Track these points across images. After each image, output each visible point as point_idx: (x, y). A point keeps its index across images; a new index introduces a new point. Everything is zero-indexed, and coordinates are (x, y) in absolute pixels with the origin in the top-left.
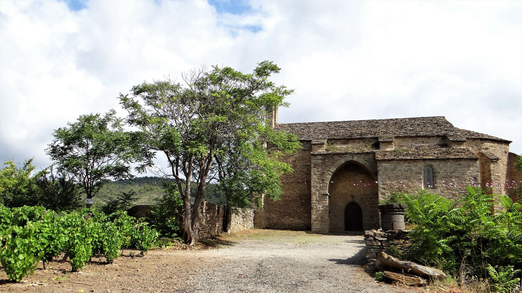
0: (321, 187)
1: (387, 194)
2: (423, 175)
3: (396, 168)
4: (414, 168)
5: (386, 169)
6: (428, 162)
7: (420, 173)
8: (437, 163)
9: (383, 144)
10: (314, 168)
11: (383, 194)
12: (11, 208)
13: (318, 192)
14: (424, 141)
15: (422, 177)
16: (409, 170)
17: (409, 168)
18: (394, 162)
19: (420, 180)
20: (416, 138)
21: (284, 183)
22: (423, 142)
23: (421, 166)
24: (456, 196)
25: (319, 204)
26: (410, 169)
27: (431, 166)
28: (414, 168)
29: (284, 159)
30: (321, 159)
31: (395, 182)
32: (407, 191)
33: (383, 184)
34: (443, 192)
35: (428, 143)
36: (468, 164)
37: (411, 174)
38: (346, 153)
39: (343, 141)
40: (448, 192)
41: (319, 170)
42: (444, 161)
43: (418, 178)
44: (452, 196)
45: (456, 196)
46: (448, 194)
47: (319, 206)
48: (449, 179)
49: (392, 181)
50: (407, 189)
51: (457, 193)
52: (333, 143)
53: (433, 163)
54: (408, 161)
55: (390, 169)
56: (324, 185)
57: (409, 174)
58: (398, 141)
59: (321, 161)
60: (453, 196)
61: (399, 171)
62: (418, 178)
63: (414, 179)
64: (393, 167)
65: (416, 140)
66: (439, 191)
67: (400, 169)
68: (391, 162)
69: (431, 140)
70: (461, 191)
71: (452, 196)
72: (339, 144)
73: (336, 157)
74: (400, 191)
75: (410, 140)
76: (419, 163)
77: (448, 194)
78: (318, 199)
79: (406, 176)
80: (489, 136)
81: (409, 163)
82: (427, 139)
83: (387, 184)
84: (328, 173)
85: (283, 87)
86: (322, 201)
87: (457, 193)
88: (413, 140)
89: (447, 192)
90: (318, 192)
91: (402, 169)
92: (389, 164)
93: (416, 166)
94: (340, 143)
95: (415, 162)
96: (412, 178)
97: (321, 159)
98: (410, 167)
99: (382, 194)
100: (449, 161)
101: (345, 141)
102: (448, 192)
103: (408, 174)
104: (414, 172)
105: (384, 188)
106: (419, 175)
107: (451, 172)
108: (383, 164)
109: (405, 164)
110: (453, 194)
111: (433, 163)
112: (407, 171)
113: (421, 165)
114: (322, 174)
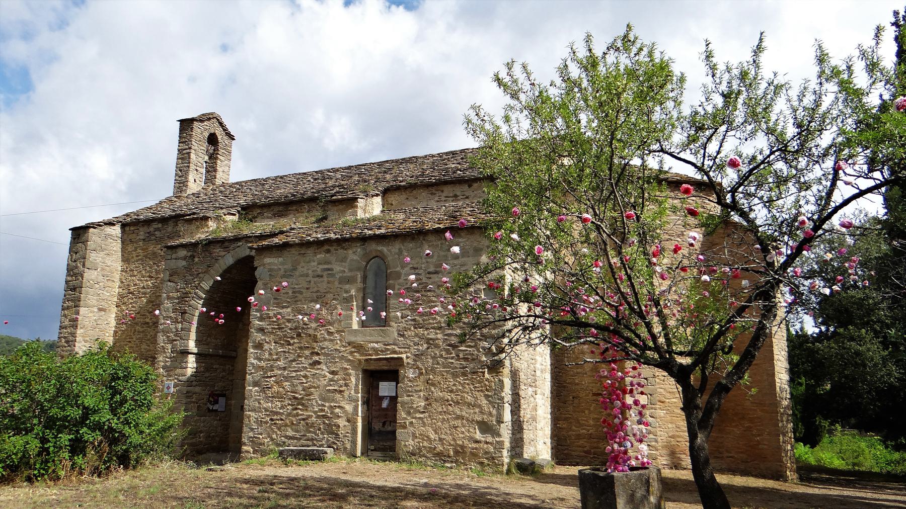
0: (177, 331)
1: (266, 346)
2: (360, 285)
3: (295, 269)
4: (337, 268)
5: (272, 274)
6: (373, 247)
7: (350, 281)
8: (396, 246)
9: (335, 208)
10: (170, 281)
11: (259, 346)
12: (896, 440)
13: (169, 346)
14: (458, 194)
15: (353, 292)
16: (325, 273)
17: (326, 266)
18: (293, 251)
19: (348, 300)
20: (440, 188)
21: (148, 323)
22: (456, 196)
23: (355, 258)
24: (437, 346)
25: (171, 376)
26: (329, 269)
27: (381, 257)
28: (337, 268)
29: (154, 264)
30: (185, 258)
31: (289, 310)
32: (315, 336)
33: (261, 319)
34: (403, 336)
35: (467, 198)
36: (475, 244)
37: (329, 285)
38: (237, 239)
39: (276, 209)
40: (417, 335)
41: (179, 287)
42: (413, 239)
43: (345, 295)
44: (425, 346)
45: (437, 346)
46: (416, 339)
47: (169, 382)
48: (424, 293)
49: (283, 307)
50: (316, 329)
51: (439, 336)
52: (256, 217)
53: (385, 249)
54: (326, 247)
55: (282, 272)
56: (186, 325)
57: (325, 285)
58: (398, 198)
59: (184, 263)
60: (428, 348)
61: (301, 276)
62: (345, 295)
63: (334, 299)
64: (288, 266)
65: (440, 194)
66: (393, 330)
67: (305, 271)
68: (286, 253)
69: (476, 190)
70: (450, 331)
71: (425, 346)
72: (268, 218)
73: (217, 251)
74: (299, 335)
75: (424, 194)
76: (350, 252)
77: (416, 339)
78: (168, 364)
79: (317, 291)
80: (681, 176)
81: (328, 251)
82: (466, 187)
83: (270, 318)
84: (196, 294)
85: (469, 122)
86: (176, 368)
87: (439, 336)
88: (432, 194)
89: (413, 333)
90: (169, 346)
91: (310, 272)
92: (281, 259)
93: (344, 260)
94: (270, 215)
95: (343, 248)
96: (330, 296)
97: (185, 258)
98: (329, 263)
99: (255, 347)
100: (426, 238)
101: (281, 208)
102: (417, 335)
103: (323, 286)
104: (338, 276)
105: (261, 330)
106: (347, 287)
107: (429, 273)
108: (268, 260)
109: (318, 256)
110: (428, 341)
111: (385, 249)
112: (322, 276)
113: (354, 254)
114: (184, 298)
